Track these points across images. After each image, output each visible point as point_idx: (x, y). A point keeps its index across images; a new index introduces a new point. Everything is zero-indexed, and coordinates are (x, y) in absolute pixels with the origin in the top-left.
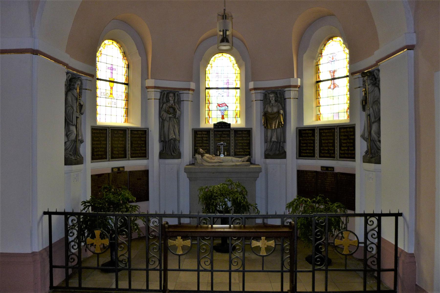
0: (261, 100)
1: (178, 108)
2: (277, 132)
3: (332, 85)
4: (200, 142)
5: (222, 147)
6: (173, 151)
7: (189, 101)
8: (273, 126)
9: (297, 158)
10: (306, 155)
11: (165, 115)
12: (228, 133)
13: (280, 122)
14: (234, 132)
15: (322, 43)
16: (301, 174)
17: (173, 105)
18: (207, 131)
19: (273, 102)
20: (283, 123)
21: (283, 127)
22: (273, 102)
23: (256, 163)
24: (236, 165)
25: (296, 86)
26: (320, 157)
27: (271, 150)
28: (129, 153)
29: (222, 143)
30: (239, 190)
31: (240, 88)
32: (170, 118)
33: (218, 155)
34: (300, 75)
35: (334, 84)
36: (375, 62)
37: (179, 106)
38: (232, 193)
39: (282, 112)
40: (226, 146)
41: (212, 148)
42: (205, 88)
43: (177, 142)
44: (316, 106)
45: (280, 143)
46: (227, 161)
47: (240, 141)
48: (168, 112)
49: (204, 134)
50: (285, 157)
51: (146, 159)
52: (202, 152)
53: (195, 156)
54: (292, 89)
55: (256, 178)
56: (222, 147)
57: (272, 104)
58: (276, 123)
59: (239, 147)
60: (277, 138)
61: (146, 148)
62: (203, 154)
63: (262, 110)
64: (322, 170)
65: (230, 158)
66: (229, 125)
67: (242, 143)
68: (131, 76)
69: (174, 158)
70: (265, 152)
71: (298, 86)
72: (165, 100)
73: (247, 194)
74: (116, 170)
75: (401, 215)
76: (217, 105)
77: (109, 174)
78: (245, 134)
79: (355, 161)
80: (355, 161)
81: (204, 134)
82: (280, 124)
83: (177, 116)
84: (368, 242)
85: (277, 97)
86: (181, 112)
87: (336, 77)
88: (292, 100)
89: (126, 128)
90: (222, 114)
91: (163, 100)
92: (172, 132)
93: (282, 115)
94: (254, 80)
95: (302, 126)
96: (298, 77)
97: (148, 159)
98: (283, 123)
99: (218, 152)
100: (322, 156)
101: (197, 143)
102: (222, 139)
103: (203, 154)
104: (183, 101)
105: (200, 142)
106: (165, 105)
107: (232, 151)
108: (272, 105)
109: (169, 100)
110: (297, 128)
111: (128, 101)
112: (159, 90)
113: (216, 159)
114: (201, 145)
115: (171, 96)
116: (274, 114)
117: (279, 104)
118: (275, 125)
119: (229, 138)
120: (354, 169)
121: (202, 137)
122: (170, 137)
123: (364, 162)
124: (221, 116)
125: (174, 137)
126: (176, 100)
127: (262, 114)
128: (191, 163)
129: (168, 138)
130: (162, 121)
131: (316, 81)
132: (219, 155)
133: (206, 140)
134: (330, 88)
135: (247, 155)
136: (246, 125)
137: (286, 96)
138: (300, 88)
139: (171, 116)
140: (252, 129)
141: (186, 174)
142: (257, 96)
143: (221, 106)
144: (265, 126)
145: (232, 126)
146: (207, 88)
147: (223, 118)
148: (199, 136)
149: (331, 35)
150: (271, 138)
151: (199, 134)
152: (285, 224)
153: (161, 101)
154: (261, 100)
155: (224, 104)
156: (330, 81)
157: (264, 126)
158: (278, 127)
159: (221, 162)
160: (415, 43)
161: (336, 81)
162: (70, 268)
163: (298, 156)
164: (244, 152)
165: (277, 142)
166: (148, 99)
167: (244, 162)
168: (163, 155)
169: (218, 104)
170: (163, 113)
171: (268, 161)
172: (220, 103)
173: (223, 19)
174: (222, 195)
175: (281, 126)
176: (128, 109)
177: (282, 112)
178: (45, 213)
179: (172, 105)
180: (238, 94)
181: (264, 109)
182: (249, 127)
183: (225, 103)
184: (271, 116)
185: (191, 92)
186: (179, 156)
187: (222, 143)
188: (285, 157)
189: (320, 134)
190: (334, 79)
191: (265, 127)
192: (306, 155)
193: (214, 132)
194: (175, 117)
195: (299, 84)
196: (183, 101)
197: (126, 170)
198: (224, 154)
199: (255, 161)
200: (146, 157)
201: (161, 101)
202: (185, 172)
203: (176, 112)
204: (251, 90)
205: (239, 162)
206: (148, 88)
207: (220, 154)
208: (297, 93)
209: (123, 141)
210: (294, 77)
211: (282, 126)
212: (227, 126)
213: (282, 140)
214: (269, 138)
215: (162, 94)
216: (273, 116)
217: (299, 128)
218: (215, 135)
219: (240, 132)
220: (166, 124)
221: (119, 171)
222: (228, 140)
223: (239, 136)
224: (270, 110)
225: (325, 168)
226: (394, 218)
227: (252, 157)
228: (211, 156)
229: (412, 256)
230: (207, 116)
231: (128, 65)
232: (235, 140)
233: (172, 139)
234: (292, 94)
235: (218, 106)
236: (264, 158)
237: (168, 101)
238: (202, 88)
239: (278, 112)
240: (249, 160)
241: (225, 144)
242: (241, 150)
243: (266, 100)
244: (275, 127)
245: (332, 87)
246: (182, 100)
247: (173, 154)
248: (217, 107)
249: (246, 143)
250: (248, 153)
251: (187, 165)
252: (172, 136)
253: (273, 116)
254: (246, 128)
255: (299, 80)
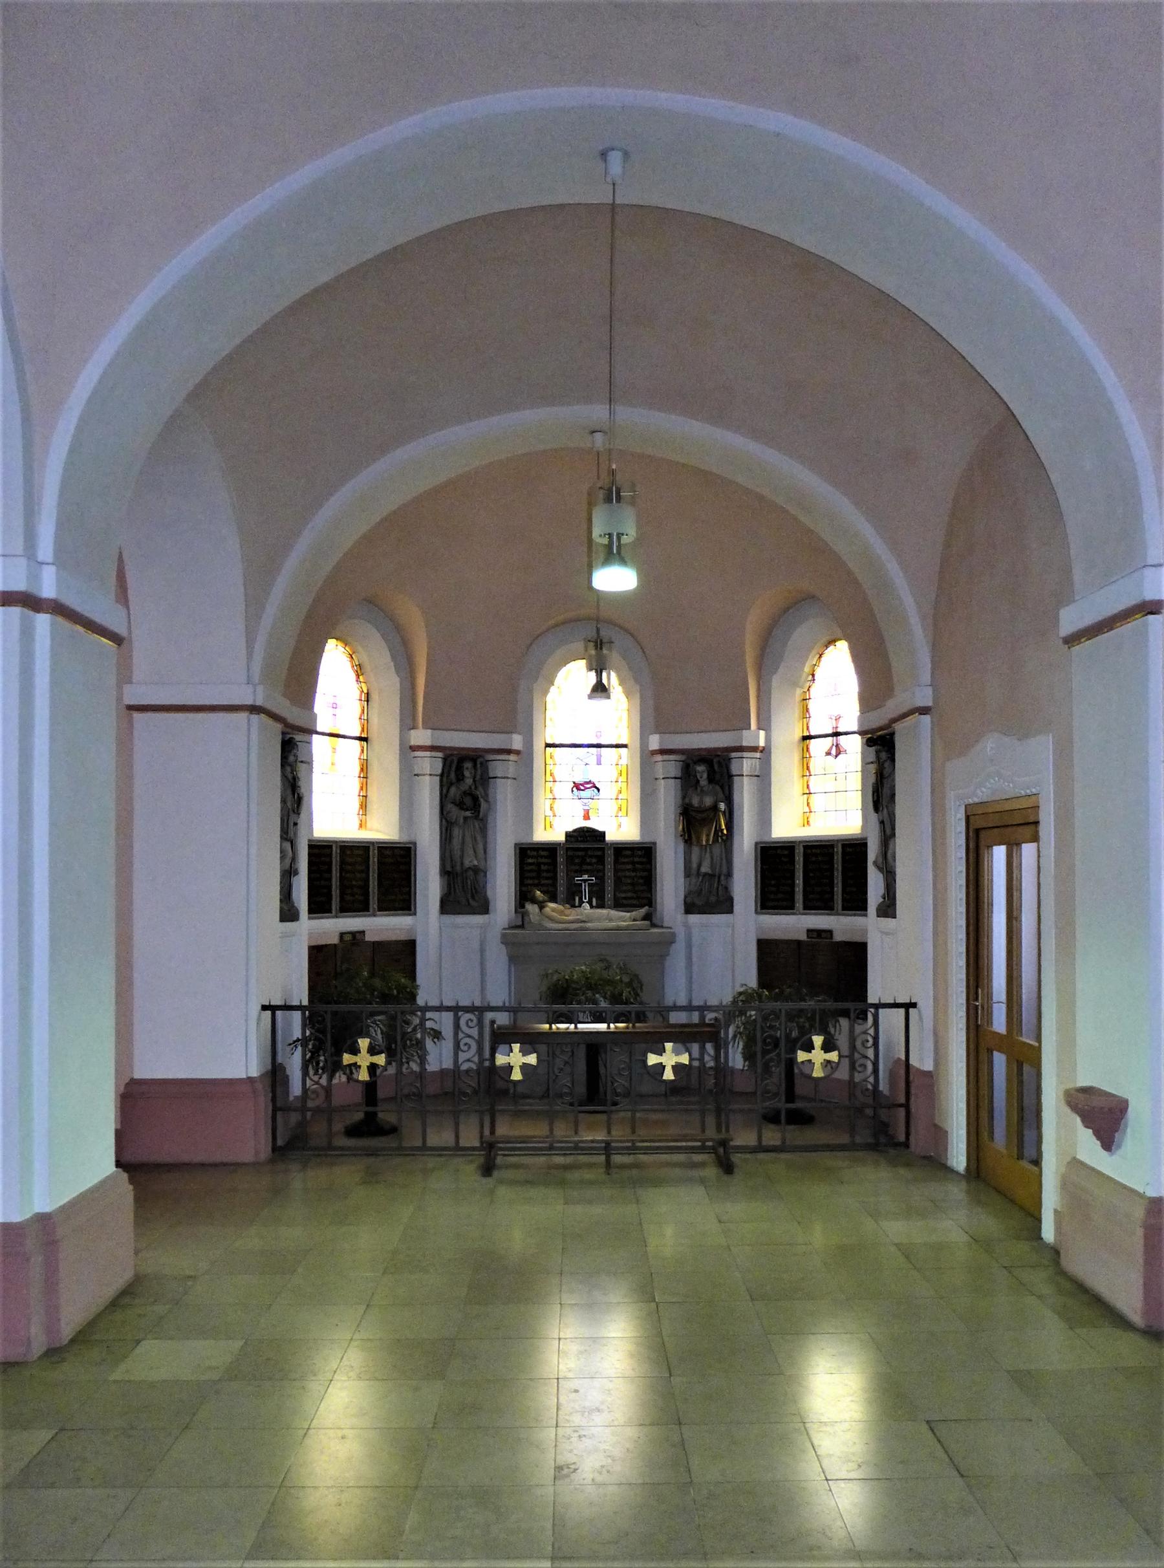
0: (675, 778)
1: (483, 794)
2: (711, 852)
3: (834, 748)
4: (534, 874)
5: (585, 886)
6: (473, 897)
7: (508, 778)
8: (704, 839)
9: (756, 912)
10: (776, 903)
11: (455, 812)
12: (599, 853)
13: (718, 830)
14: (612, 851)
15: (814, 652)
16: (765, 946)
17: (473, 787)
18: (550, 849)
19: (704, 782)
20: (725, 832)
21: (727, 840)
22: (704, 782)
23: (665, 924)
24: (618, 929)
25: (754, 749)
26: (805, 908)
27: (699, 893)
28: (335, 904)
29: (586, 877)
30: (626, 979)
31: (629, 745)
32: (466, 818)
33: (577, 904)
34: (765, 724)
35: (837, 746)
36: (887, 722)
37: (485, 791)
38: (610, 982)
39: (722, 806)
40: (596, 884)
41: (561, 889)
42: (544, 745)
43: (482, 874)
44: (802, 793)
45: (719, 878)
46: (599, 919)
47: (628, 874)
48: (461, 805)
49: (542, 857)
50: (730, 910)
51: (410, 915)
52: (541, 899)
53: (523, 906)
54: (745, 754)
55: (663, 957)
56: (586, 888)
57: (702, 787)
58: (710, 832)
59: (624, 888)
60: (712, 866)
61: (411, 887)
62: (544, 902)
63: (680, 801)
64: (808, 936)
65: (604, 911)
66: (603, 834)
67: (633, 878)
68: (375, 720)
69: (474, 912)
70: (686, 897)
71: (760, 749)
72: (453, 775)
73: (641, 989)
74: (348, 938)
75: (914, 1005)
76: (573, 785)
77: (335, 945)
78: (640, 856)
79: (866, 915)
80: (866, 915)
81: (542, 857)
82: (720, 834)
83: (481, 814)
84: (856, 1055)
85: (714, 771)
86: (489, 805)
87: (840, 730)
88: (745, 779)
89: (367, 842)
90: (587, 808)
91: (448, 776)
92: (471, 852)
93: (724, 813)
94: (659, 729)
95: (766, 839)
96: (759, 729)
97: (415, 914)
98: (725, 832)
99: (577, 899)
100: (811, 906)
101: (527, 878)
102: (585, 867)
103: (544, 902)
104: (495, 778)
105: (534, 874)
106: (453, 790)
107: (609, 896)
108: (702, 791)
109: (463, 775)
110: (756, 844)
111: (366, 778)
112: (440, 754)
113: (572, 914)
114: (536, 882)
115: (467, 768)
116: (706, 810)
117: (718, 788)
118: (708, 835)
119: (602, 867)
120: (865, 932)
121: (539, 864)
122: (467, 863)
123: (878, 916)
124: (582, 813)
125: (476, 863)
126: (478, 777)
127: (679, 811)
128: (514, 924)
129: (462, 864)
130: (447, 826)
131: (801, 735)
132: (580, 906)
133: (548, 871)
134: (828, 753)
135: (642, 906)
136: (642, 834)
137: (734, 770)
138: (766, 751)
139: (468, 814)
140: (655, 844)
141: (503, 947)
142: (669, 767)
143: (582, 788)
144: (686, 838)
145: (608, 838)
146: (548, 745)
147: (587, 817)
148: (530, 861)
149: (833, 638)
150: (699, 866)
151: (532, 857)
152: (707, 1021)
153: (445, 779)
154: (675, 778)
155: (589, 782)
156: (830, 738)
157: (684, 839)
158: (715, 840)
159: (584, 922)
160: (930, 704)
161: (841, 738)
162: (310, 1110)
163: (759, 908)
164: (638, 898)
165: (712, 876)
166: (415, 775)
167: (637, 921)
168: (448, 905)
169: (574, 783)
170: (450, 807)
171: (694, 919)
172: (579, 780)
173: (596, 649)
174: (590, 987)
175: (722, 839)
176: (366, 797)
177: (722, 806)
178: (265, 1008)
179: (470, 788)
180: (624, 761)
181: (684, 798)
182: (647, 840)
183: (593, 780)
184: (699, 816)
185: (512, 757)
186: (484, 908)
187: (586, 877)
188: (730, 910)
189: (806, 856)
190: (836, 734)
191: (686, 842)
192: (776, 903)
193: (567, 851)
194: (477, 817)
195: (762, 743)
196: (495, 778)
197: (368, 938)
198: (590, 902)
199: (662, 920)
200: (410, 910)
201: (445, 779)
202: (502, 943)
203: (480, 806)
204: (654, 753)
205: (624, 921)
206: (414, 748)
207: (581, 902)
208: (758, 764)
209: (362, 871)
210: (750, 728)
211: (724, 838)
212: (596, 836)
213: (725, 870)
214: (695, 866)
215: (448, 763)
216: (704, 815)
217: (761, 843)
218: (570, 860)
219: (628, 853)
220: (456, 832)
221: (354, 939)
222: (599, 871)
223: (626, 860)
224: (695, 802)
225: (815, 933)
226: (902, 1011)
227: (655, 910)
228: (561, 907)
229: (928, 1074)
230: (549, 813)
231: (368, 694)
232: (616, 871)
233: (469, 868)
234: (747, 765)
235: (575, 789)
236: (683, 912)
237: (460, 778)
238: (538, 746)
239: (715, 808)
240: (647, 917)
241: (592, 880)
242: (629, 895)
243: (687, 779)
244: (707, 840)
245: (834, 752)
246: (491, 775)
247: (471, 901)
248: (572, 791)
249: (642, 877)
250: (645, 901)
251: (504, 929)
252: (470, 862)
253: (704, 815)
254: (641, 841)
255: (762, 733)
